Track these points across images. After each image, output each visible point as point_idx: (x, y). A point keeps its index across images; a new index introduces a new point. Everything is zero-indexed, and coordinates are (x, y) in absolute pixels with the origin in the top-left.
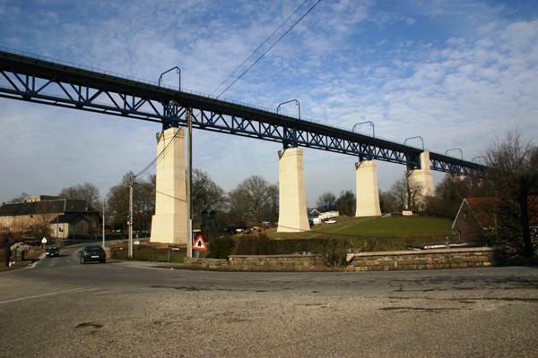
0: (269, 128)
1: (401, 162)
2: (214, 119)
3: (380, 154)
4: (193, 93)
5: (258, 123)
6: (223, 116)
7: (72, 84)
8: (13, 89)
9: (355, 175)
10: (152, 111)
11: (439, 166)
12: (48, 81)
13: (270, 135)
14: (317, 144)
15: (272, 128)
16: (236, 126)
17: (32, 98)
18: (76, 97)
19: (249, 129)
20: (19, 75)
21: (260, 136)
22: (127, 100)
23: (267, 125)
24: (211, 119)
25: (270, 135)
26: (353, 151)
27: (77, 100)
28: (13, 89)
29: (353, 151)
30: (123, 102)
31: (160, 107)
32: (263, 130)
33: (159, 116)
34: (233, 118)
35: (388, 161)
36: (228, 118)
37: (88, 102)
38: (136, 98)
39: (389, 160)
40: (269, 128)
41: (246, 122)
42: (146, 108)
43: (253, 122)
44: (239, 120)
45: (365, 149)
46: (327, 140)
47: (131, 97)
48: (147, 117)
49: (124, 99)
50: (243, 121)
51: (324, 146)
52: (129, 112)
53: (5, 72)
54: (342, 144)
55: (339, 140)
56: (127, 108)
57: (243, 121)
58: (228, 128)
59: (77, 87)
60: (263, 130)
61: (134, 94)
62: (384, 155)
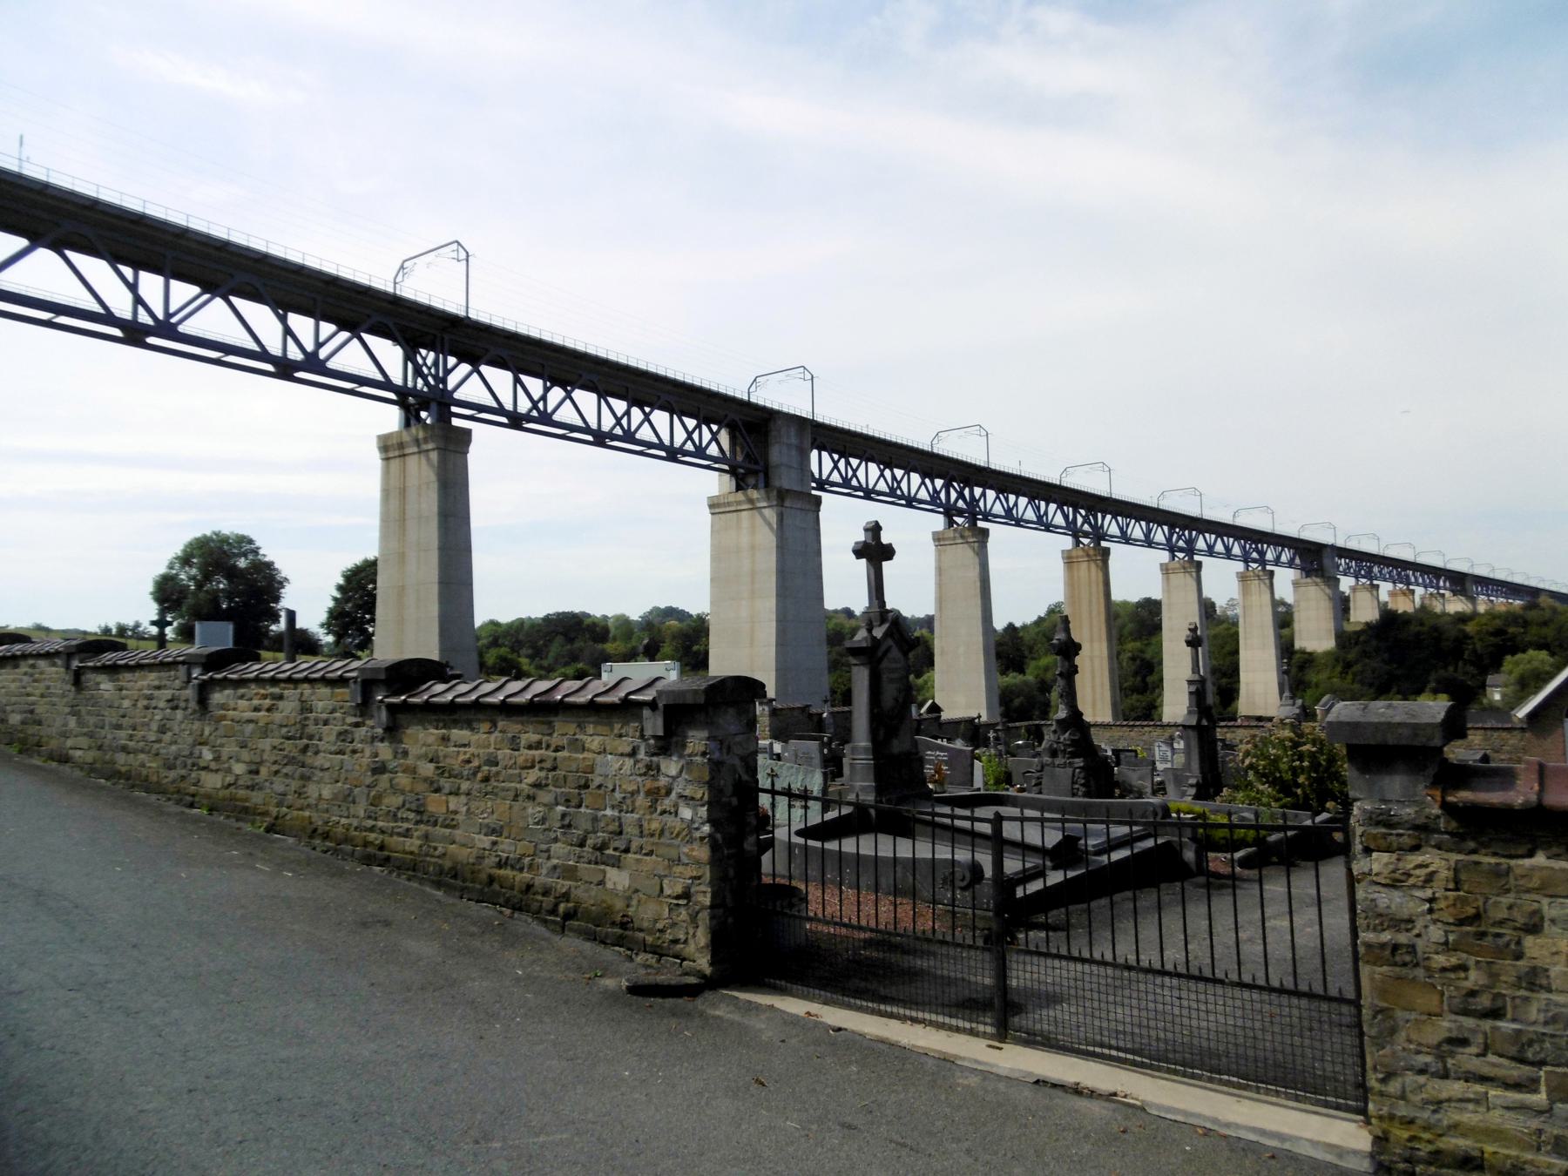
0: (627, 413)
1: (1048, 527)
2: (452, 381)
3: (923, 495)
4: (785, 410)
5: (594, 396)
6: (484, 369)
7: (114, 259)
8: (97, 308)
9: (940, 601)
10: (236, 335)
11: (1219, 547)
12: (22, 243)
13: (546, 418)
14: (846, 483)
15: (636, 412)
16: (524, 406)
17: (297, 375)
18: (121, 305)
19: (566, 414)
20: (121, 267)
21: (600, 439)
22: (143, 291)
23: (620, 406)
24: (544, 398)
25: (629, 436)
26: (892, 493)
27: (128, 315)
28: (518, 386)
29: (892, 493)
30: (129, 296)
31: (390, 354)
32: (608, 422)
33: (387, 384)
34: (517, 381)
35: (1047, 530)
36: (501, 379)
37: (166, 328)
38: (175, 285)
39: (1019, 522)
40: (627, 413)
41: (556, 394)
42: (351, 357)
43: (578, 394)
44: (535, 385)
45: (961, 495)
46: (870, 473)
47: (159, 280)
48: (356, 384)
49: (133, 287)
50: (547, 390)
51: (860, 488)
52: (149, 331)
53: (233, 299)
54: (861, 473)
55: (854, 462)
56: (144, 318)
57: (547, 390)
58: (586, 429)
59: (128, 272)
60: (680, 436)
61: (172, 271)
62: (1009, 511)
